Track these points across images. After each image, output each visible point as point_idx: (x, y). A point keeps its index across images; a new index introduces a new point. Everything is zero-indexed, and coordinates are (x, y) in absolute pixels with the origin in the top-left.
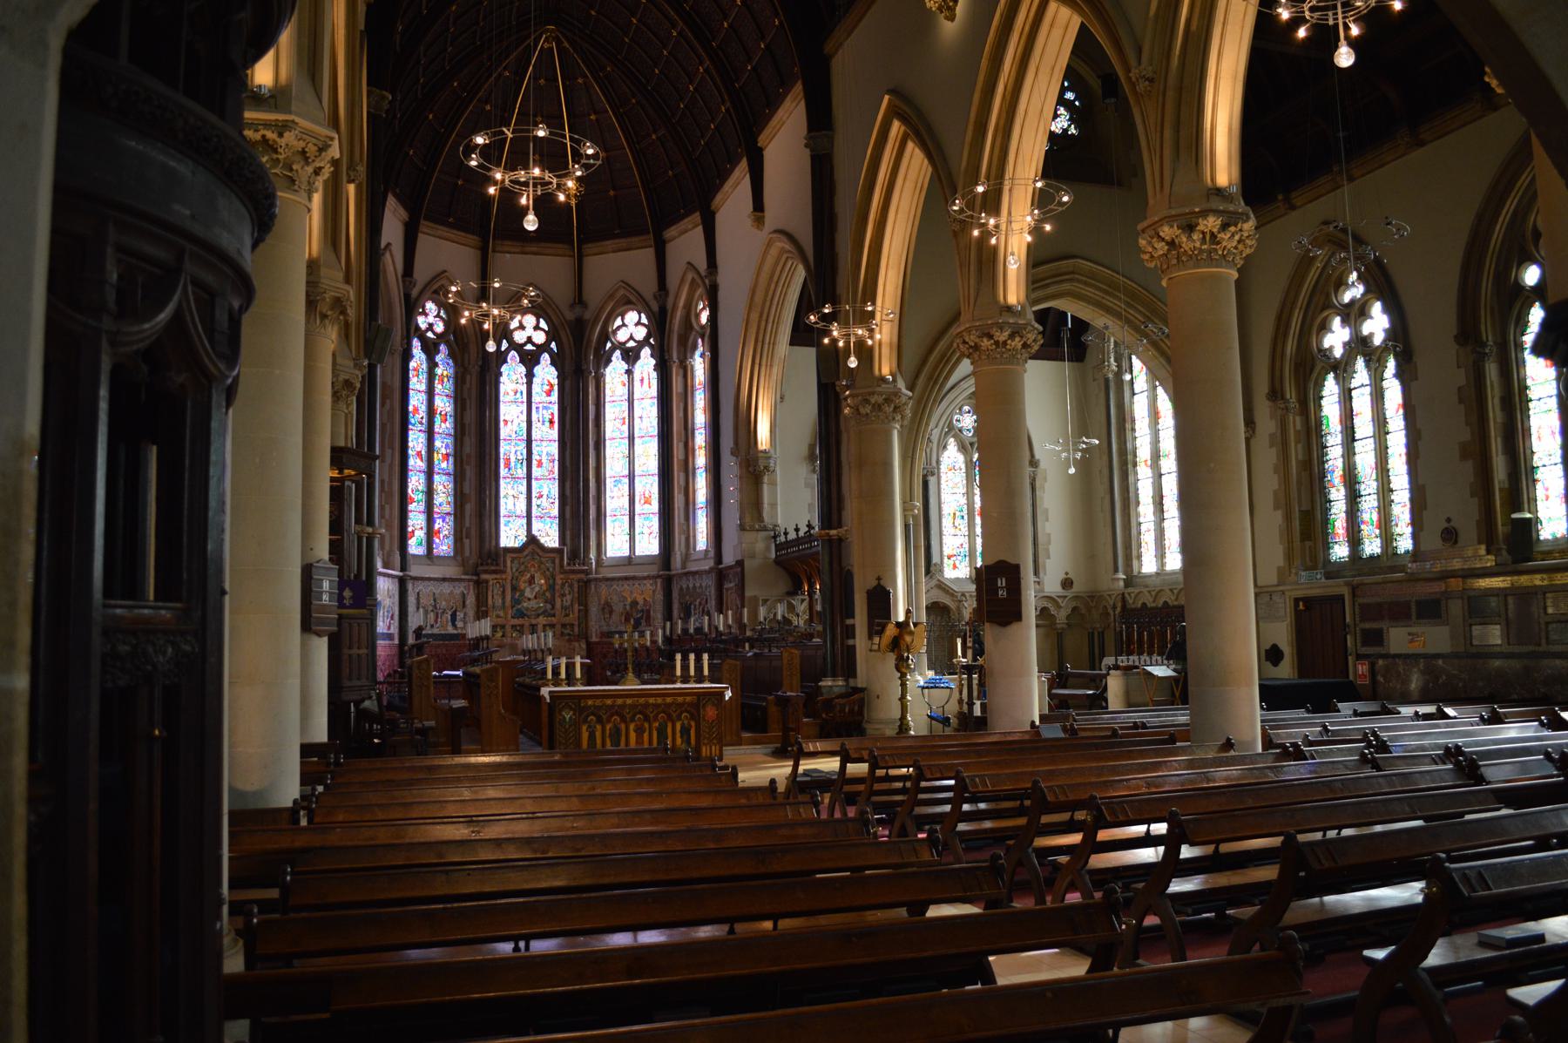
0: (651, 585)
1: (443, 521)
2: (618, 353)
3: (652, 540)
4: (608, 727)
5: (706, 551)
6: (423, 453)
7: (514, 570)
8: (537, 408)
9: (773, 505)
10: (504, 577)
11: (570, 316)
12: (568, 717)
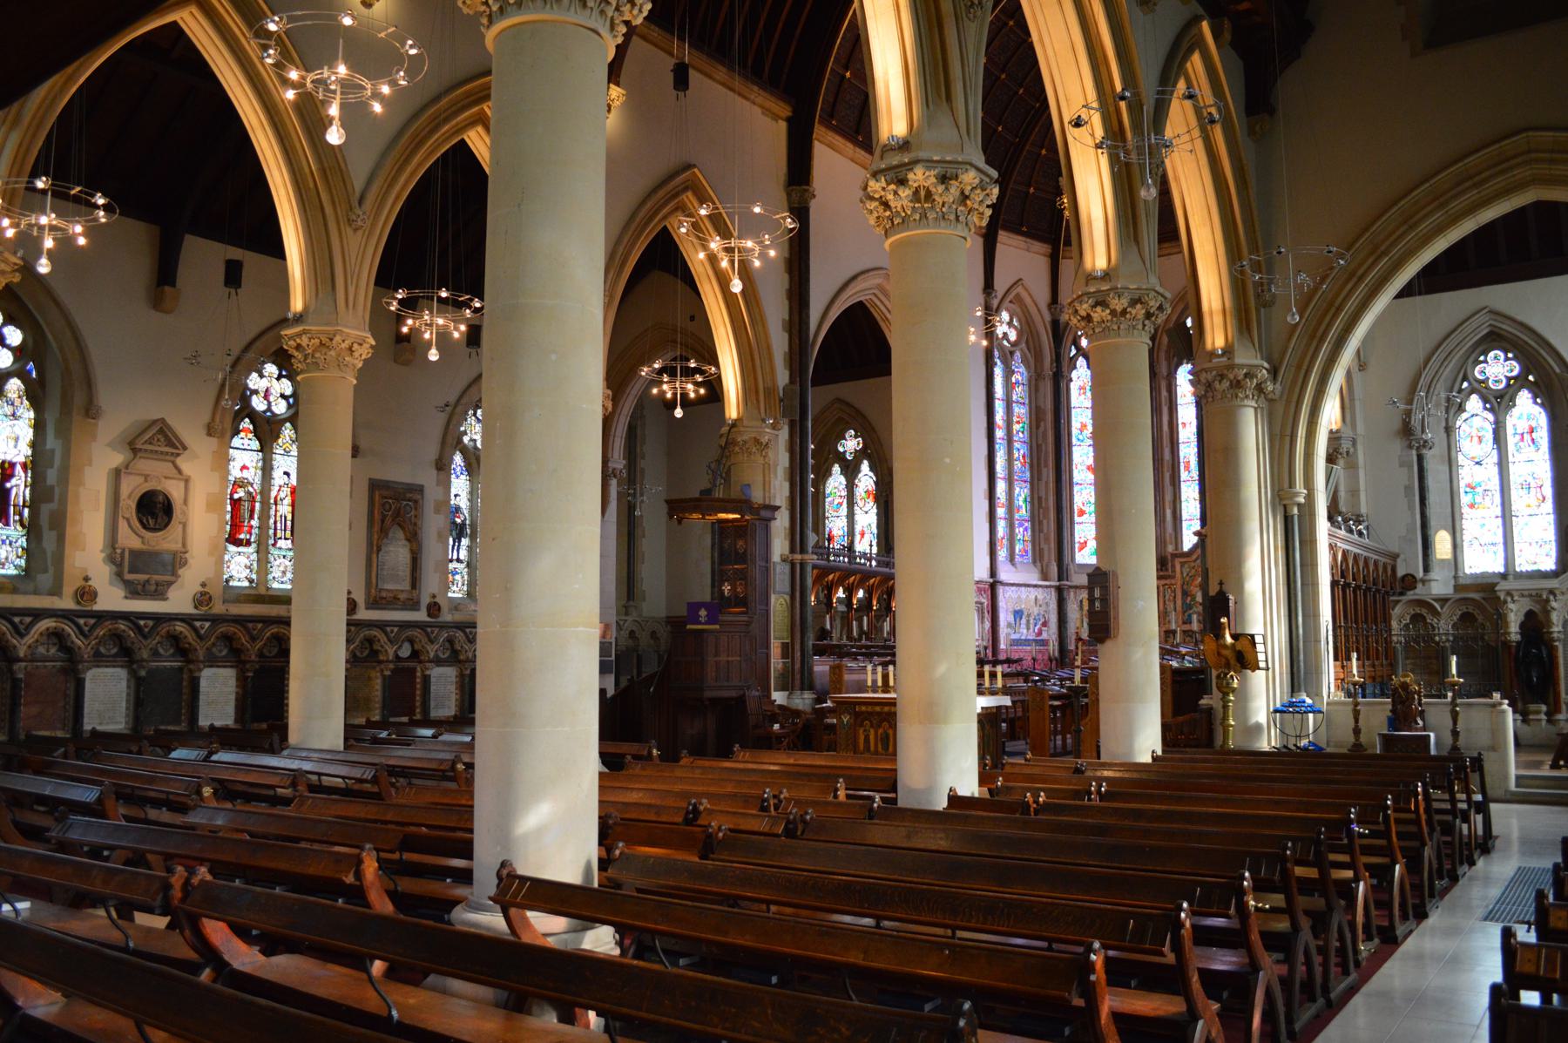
4: (880, 731)
10: (1173, 582)
12: (845, 720)
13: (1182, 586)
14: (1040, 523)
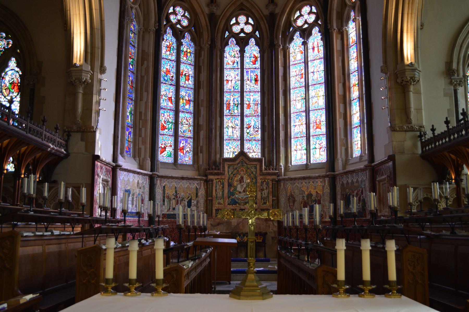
0: (321, 182)
1: (186, 142)
2: (298, 34)
3: (322, 153)
5: (361, 156)
6: (173, 99)
7: (230, 173)
8: (247, 72)
9: (419, 110)
10: (223, 177)
11: (266, 12)
13: (228, 180)
14: (140, 130)
